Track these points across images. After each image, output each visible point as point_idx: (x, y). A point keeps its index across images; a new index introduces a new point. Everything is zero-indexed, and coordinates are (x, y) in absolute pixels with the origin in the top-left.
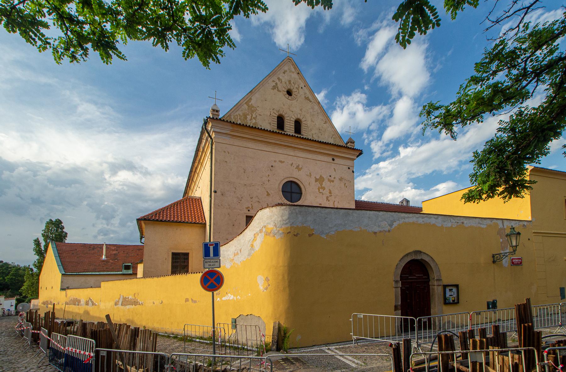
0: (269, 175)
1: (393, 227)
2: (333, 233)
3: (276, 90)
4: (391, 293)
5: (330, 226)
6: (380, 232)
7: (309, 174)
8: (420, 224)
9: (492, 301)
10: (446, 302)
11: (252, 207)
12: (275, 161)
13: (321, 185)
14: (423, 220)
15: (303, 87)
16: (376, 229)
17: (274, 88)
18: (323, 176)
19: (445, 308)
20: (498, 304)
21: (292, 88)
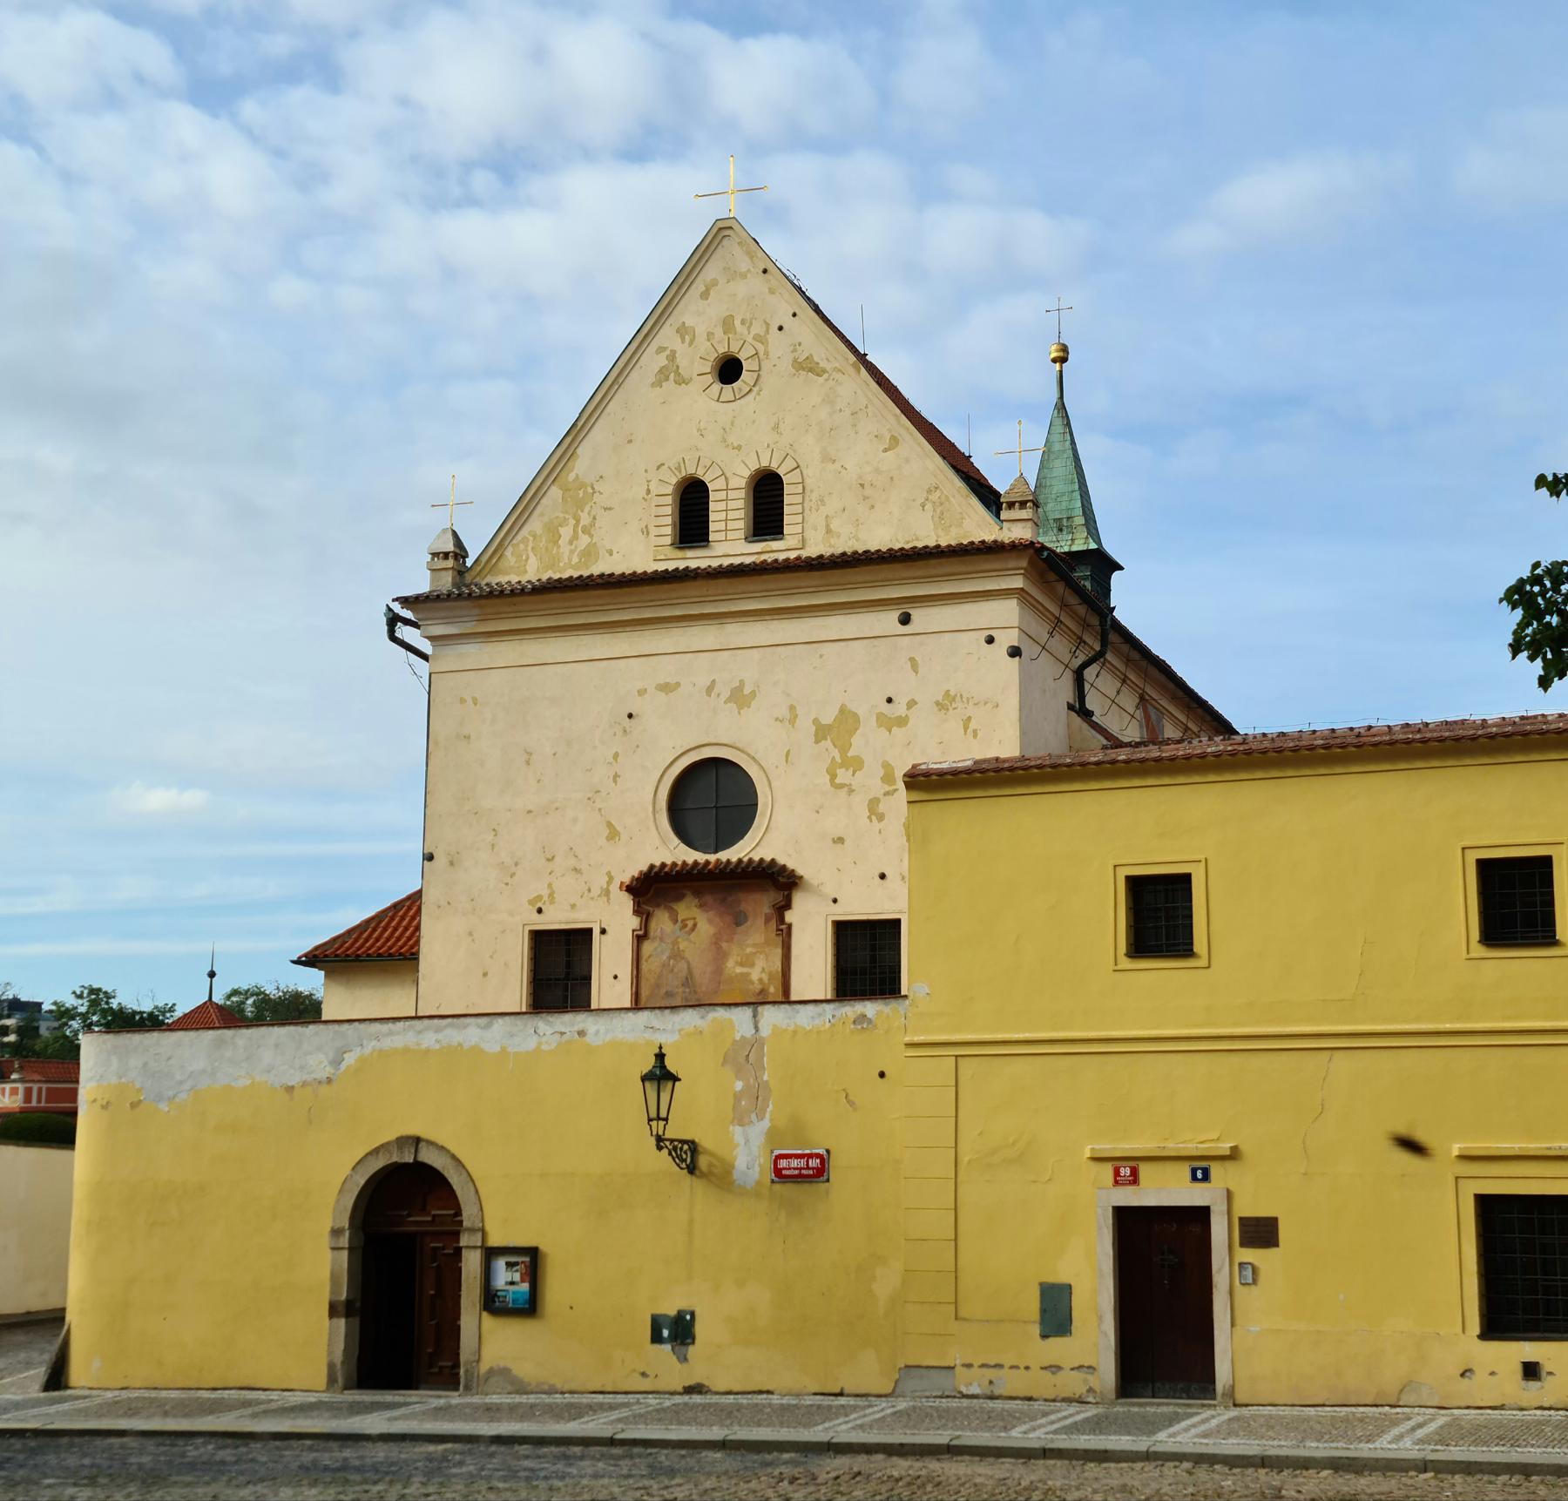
0: (616, 755)
1: (344, 1065)
2: (183, 1096)
3: (669, 385)
4: (319, 1264)
5: (178, 1077)
6: (304, 1084)
7: (783, 712)
8: (427, 1051)
9: (673, 1312)
10: (492, 1303)
11: (551, 895)
12: (642, 692)
13: (844, 750)
14: (440, 1036)
15: (788, 322)
16: (295, 1079)
17: (663, 375)
18: (852, 707)
19: (488, 1321)
20: (699, 1329)
21: (734, 349)
